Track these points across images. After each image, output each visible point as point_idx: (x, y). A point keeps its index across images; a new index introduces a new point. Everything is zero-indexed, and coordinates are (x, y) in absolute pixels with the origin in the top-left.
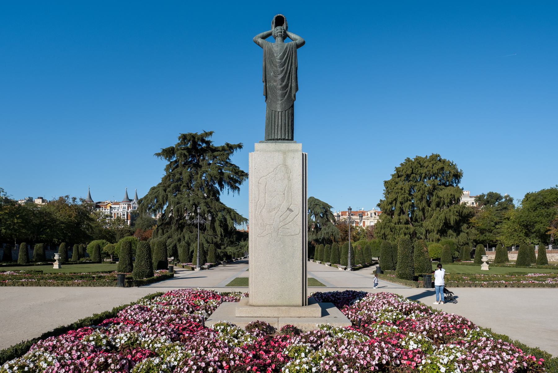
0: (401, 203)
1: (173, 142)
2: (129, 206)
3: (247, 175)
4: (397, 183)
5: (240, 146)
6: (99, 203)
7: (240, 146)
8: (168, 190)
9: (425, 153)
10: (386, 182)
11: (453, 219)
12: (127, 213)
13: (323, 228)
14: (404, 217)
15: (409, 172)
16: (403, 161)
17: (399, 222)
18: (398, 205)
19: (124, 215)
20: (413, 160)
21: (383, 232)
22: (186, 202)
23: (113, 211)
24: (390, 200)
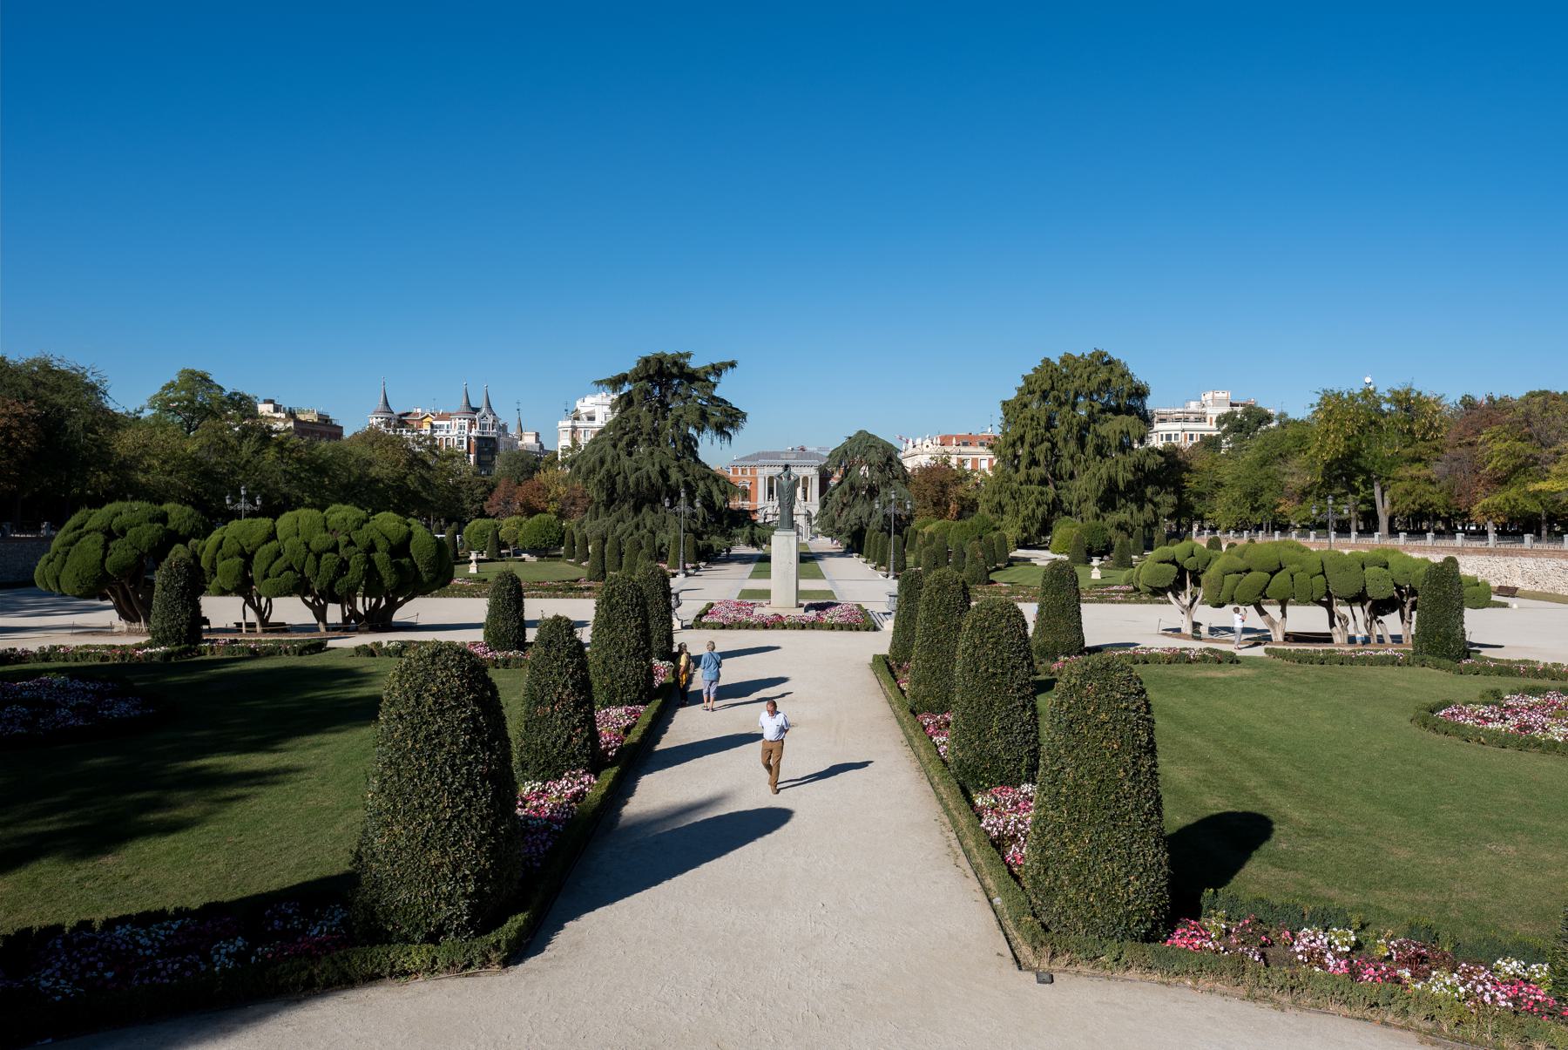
0: (1032, 446)
1: (628, 365)
2: (472, 422)
3: (744, 416)
4: (1026, 406)
5: (733, 365)
6: (407, 414)
7: (733, 365)
8: (620, 445)
9: (1082, 348)
10: (1004, 403)
11: (1123, 476)
12: (469, 438)
13: (882, 491)
14: (1038, 472)
15: (1046, 386)
16: (1038, 364)
17: (1029, 481)
18: (1026, 447)
19: (461, 442)
20: (1058, 362)
21: (996, 500)
22: (649, 467)
23: (438, 434)
24: (1010, 439)
